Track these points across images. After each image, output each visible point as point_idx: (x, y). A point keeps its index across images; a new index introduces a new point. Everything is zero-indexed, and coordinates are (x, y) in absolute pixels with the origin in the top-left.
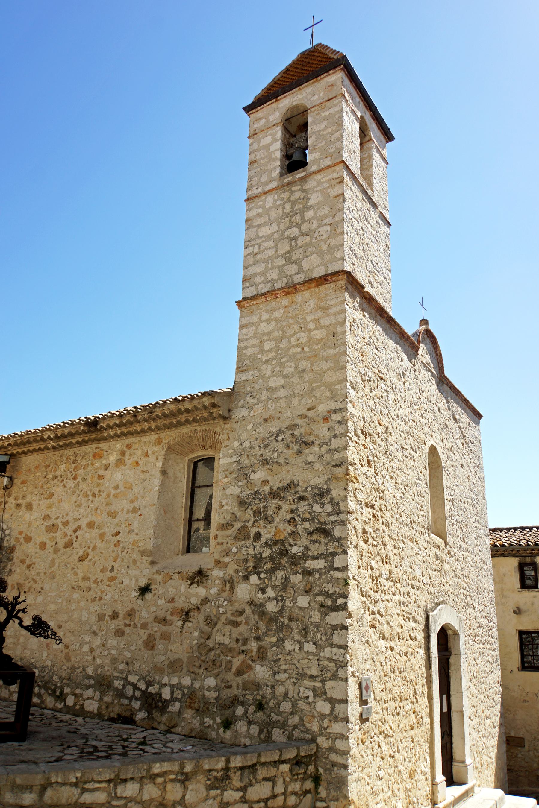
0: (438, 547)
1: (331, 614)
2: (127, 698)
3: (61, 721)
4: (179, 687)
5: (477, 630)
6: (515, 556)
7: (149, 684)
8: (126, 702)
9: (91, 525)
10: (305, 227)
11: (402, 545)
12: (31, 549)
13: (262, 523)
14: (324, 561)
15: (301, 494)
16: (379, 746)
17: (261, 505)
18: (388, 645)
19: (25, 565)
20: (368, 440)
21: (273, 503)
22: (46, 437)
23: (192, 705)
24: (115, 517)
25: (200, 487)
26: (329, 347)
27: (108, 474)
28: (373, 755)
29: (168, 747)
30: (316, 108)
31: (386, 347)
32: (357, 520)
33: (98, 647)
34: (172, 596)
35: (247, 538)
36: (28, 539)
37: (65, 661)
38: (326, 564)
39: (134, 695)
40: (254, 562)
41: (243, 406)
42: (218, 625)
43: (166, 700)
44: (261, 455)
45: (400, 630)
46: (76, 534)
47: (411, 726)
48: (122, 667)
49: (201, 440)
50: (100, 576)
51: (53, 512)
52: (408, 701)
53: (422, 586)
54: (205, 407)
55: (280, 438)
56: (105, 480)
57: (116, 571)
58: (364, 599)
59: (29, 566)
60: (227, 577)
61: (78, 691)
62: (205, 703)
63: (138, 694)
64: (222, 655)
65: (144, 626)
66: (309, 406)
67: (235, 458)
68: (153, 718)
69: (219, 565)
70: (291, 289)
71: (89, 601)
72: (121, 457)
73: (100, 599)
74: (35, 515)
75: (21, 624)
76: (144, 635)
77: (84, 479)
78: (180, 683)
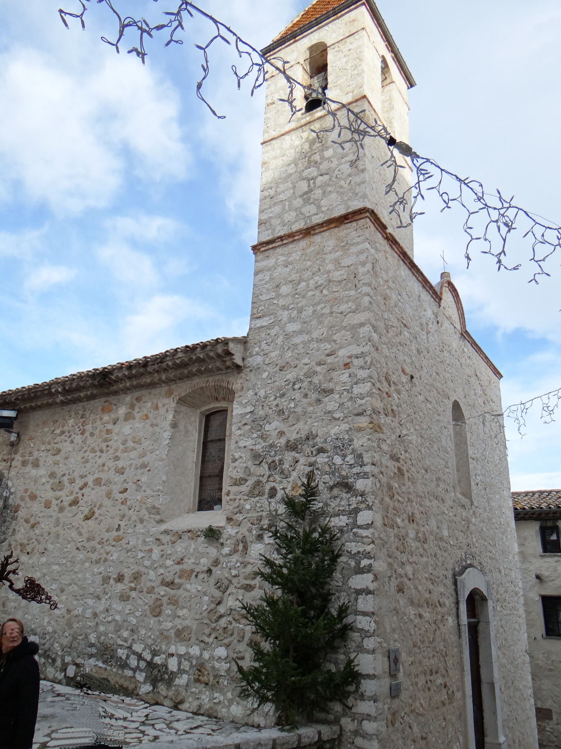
0: (463, 506)
1: (354, 576)
2: (131, 669)
3: (59, 695)
4: (187, 657)
5: (504, 596)
6: (536, 519)
7: (155, 653)
8: (129, 673)
9: (98, 482)
10: (324, 166)
11: (428, 503)
12: (36, 507)
13: (277, 477)
14: (346, 517)
15: (320, 445)
16: (410, 727)
17: (277, 458)
18: (417, 612)
19: (30, 525)
20: (392, 388)
21: (289, 456)
22: (53, 390)
23: (201, 678)
24: (123, 473)
25: (212, 441)
26: (350, 289)
27: (116, 429)
28: (403, 738)
29: (171, 728)
30: (336, 45)
31: (409, 294)
32: (382, 473)
33: (102, 612)
34: (181, 556)
35: (261, 494)
36: (33, 497)
37: (66, 628)
38: (347, 521)
39: (138, 666)
40: (269, 520)
41: (258, 354)
42: (230, 589)
43: (172, 673)
44: (277, 405)
45: (428, 596)
46: (82, 491)
47: (443, 702)
48: (126, 634)
49: (213, 391)
50: (106, 536)
51: (60, 470)
52: (439, 675)
53: (449, 548)
54: (219, 356)
55: (297, 387)
56: (114, 434)
57: (122, 530)
58: (390, 560)
59: (33, 526)
60: (240, 537)
61: (79, 661)
62: (215, 676)
63: (143, 664)
64: (234, 622)
65: (151, 590)
66: (327, 352)
67: (249, 409)
68: (158, 692)
69: (232, 523)
70: (308, 232)
71: (94, 562)
72: (130, 410)
73: (106, 560)
74: (42, 471)
75: (11, 587)
76: (150, 599)
77: (92, 434)
78: (188, 653)
